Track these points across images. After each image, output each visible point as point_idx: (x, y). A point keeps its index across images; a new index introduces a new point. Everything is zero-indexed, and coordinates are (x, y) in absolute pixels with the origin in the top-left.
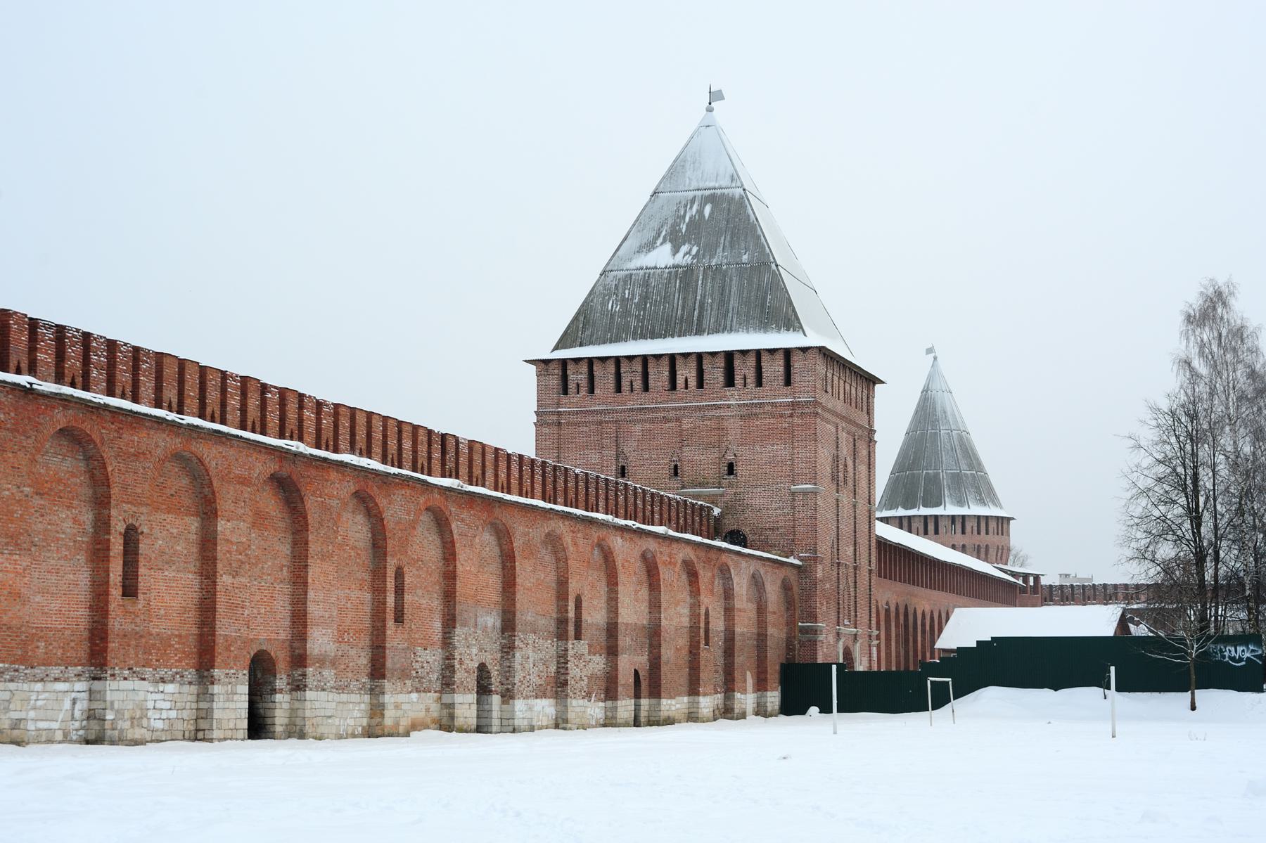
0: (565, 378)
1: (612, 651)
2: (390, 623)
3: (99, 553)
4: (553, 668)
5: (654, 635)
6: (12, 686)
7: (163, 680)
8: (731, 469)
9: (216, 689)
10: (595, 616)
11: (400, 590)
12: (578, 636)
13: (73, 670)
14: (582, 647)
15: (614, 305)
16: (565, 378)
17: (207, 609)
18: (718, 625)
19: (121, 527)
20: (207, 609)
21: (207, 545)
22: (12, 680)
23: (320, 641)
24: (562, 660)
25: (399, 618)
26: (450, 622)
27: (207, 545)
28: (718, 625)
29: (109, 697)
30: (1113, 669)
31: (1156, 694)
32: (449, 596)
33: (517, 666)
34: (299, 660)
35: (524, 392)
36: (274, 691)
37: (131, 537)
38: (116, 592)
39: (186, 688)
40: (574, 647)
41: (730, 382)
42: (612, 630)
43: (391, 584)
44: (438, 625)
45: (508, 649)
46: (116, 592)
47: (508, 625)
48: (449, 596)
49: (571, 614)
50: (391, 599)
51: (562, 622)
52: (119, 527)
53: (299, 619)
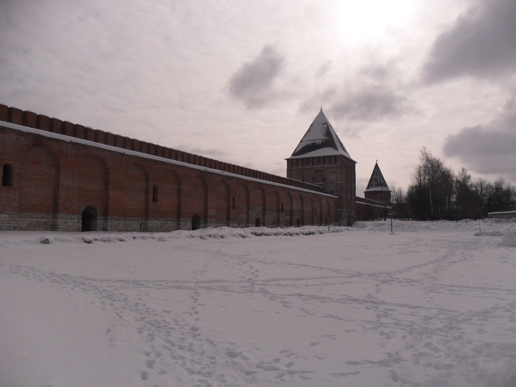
0: (292, 162)
1: (291, 215)
2: (231, 209)
3: (147, 192)
4: (276, 219)
5: (302, 212)
6: (119, 222)
7: (167, 221)
9: (181, 223)
10: (287, 208)
11: (234, 201)
12: (282, 212)
13: (139, 218)
14: (283, 214)
15: (305, 148)
16: (292, 162)
17: (179, 205)
18: (318, 210)
19: (153, 186)
20: (179, 205)
21: (179, 191)
22: (119, 220)
23: (211, 212)
24: (278, 217)
25: (234, 208)
26: (248, 209)
27: (179, 191)
28: (318, 210)
29: (149, 224)
30: (357, 202)
31: (237, 164)
32: (248, 203)
33: (266, 218)
34: (206, 216)
35: (284, 165)
36: (200, 223)
37: (155, 189)
39: (174, 223)
40: (281, 214)
41: (324, 162)
42: (291, 211)
43: (231, 200)
44: (246, 209)
45: (264, 215)
46: (151, 201)
47: (264, 210)
48: (248, 203)
49: (281, 207)
50: (231, 204)
51: (278, 209)
53: (206, 208)
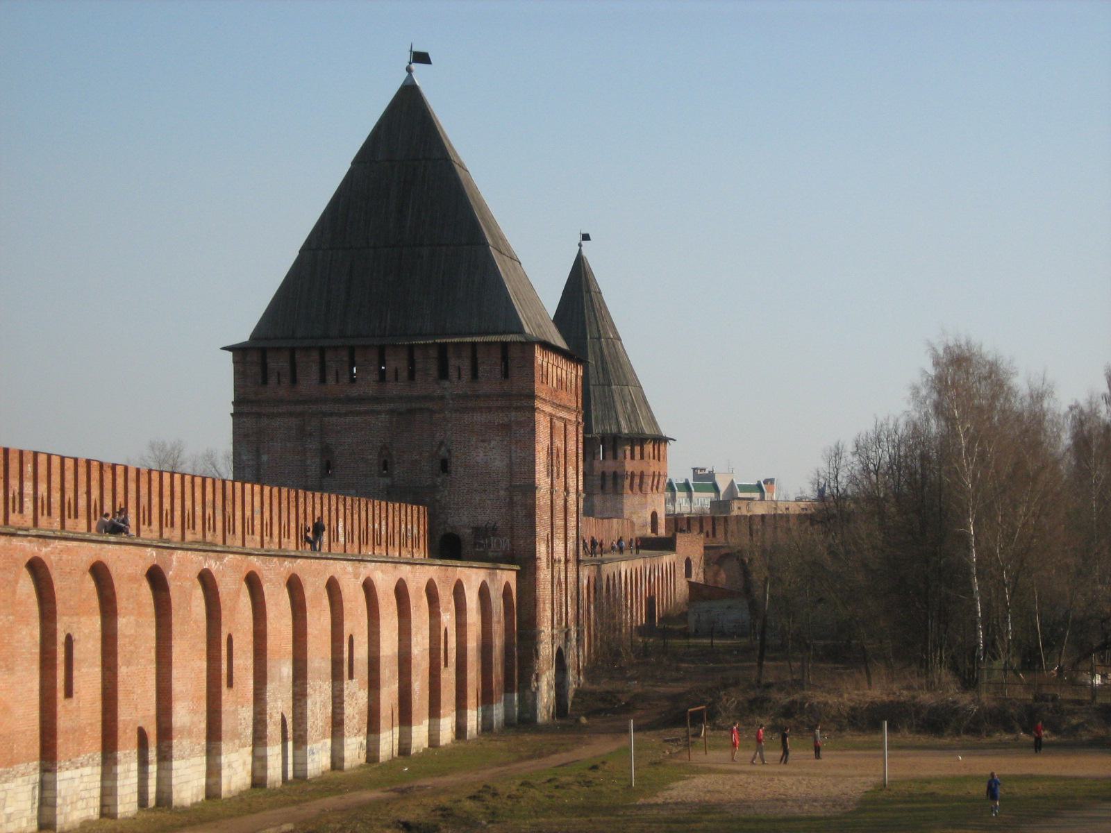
8: (445, 466)
38: (60, 694)
41: (443, 374)
46: (60, 694)
52: (61, 638)
